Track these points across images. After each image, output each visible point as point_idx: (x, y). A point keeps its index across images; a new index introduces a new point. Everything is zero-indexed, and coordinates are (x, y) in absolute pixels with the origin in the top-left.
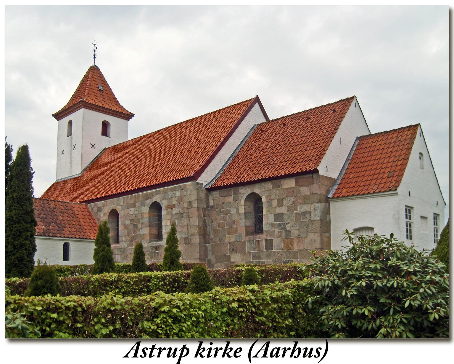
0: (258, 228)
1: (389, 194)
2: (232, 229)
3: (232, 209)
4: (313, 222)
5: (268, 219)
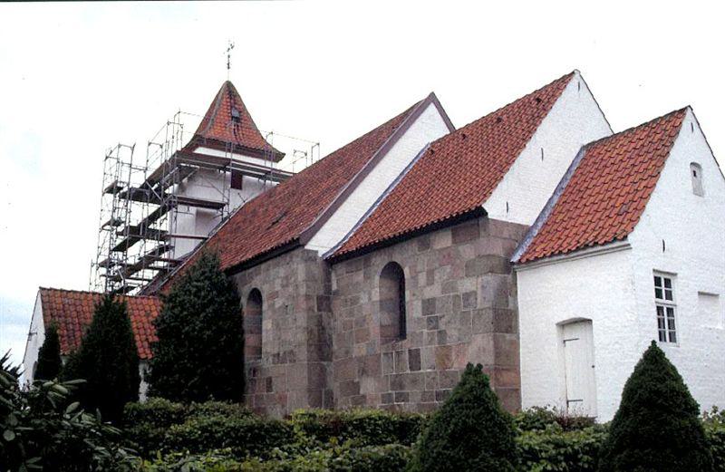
0: (400, 329)
1: (613, 248)
2: (362, 336)
3: (362, 295)
4: (479, 313)
5: (414, 310)
